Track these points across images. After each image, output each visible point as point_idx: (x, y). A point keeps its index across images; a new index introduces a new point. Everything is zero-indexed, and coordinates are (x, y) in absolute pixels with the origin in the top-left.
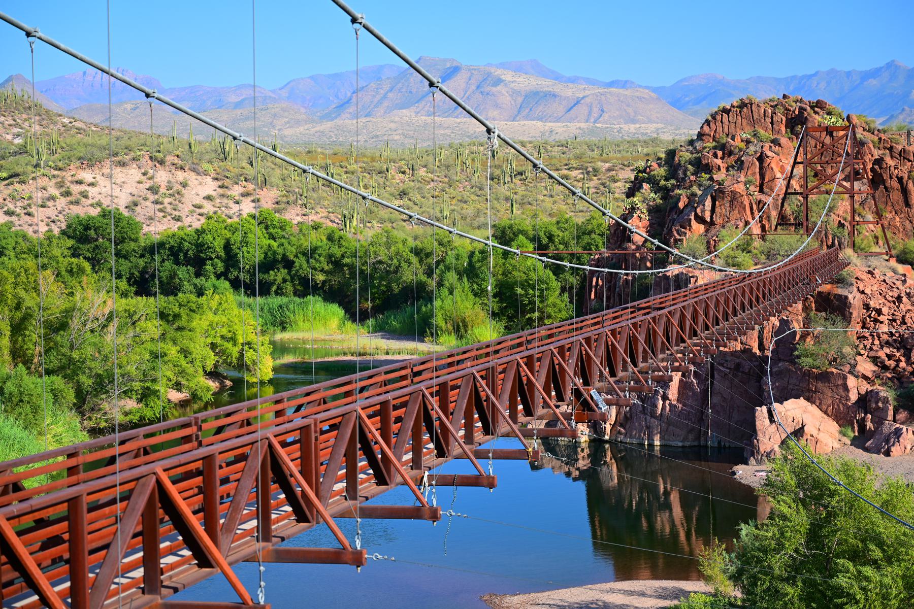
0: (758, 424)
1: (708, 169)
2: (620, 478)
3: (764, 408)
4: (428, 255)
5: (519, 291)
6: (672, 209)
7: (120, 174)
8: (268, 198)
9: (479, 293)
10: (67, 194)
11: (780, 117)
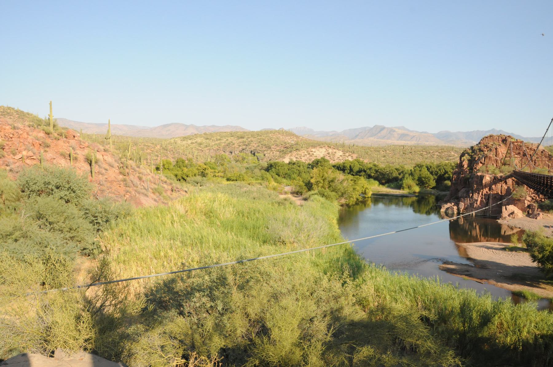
0: (503, 210)
1: (482, 151)
2: (464, 222)
3: (504, 207)
4: (399, 170)
5: (423, 179)
6: (474, 160)
7: (321, 150)
8: (355, 156)
9: (413, 179)
10: (309, 154)
11: (500, 139)
